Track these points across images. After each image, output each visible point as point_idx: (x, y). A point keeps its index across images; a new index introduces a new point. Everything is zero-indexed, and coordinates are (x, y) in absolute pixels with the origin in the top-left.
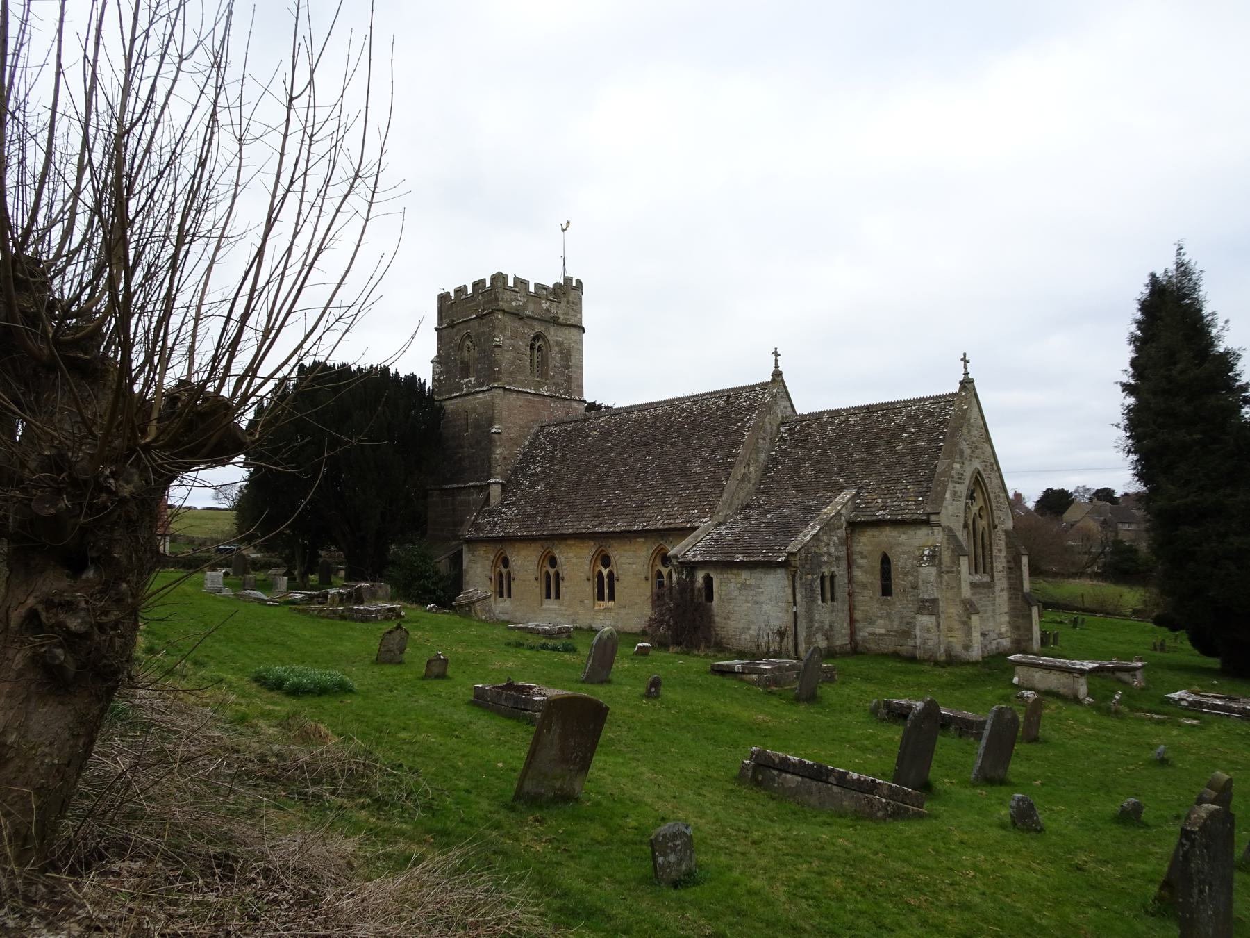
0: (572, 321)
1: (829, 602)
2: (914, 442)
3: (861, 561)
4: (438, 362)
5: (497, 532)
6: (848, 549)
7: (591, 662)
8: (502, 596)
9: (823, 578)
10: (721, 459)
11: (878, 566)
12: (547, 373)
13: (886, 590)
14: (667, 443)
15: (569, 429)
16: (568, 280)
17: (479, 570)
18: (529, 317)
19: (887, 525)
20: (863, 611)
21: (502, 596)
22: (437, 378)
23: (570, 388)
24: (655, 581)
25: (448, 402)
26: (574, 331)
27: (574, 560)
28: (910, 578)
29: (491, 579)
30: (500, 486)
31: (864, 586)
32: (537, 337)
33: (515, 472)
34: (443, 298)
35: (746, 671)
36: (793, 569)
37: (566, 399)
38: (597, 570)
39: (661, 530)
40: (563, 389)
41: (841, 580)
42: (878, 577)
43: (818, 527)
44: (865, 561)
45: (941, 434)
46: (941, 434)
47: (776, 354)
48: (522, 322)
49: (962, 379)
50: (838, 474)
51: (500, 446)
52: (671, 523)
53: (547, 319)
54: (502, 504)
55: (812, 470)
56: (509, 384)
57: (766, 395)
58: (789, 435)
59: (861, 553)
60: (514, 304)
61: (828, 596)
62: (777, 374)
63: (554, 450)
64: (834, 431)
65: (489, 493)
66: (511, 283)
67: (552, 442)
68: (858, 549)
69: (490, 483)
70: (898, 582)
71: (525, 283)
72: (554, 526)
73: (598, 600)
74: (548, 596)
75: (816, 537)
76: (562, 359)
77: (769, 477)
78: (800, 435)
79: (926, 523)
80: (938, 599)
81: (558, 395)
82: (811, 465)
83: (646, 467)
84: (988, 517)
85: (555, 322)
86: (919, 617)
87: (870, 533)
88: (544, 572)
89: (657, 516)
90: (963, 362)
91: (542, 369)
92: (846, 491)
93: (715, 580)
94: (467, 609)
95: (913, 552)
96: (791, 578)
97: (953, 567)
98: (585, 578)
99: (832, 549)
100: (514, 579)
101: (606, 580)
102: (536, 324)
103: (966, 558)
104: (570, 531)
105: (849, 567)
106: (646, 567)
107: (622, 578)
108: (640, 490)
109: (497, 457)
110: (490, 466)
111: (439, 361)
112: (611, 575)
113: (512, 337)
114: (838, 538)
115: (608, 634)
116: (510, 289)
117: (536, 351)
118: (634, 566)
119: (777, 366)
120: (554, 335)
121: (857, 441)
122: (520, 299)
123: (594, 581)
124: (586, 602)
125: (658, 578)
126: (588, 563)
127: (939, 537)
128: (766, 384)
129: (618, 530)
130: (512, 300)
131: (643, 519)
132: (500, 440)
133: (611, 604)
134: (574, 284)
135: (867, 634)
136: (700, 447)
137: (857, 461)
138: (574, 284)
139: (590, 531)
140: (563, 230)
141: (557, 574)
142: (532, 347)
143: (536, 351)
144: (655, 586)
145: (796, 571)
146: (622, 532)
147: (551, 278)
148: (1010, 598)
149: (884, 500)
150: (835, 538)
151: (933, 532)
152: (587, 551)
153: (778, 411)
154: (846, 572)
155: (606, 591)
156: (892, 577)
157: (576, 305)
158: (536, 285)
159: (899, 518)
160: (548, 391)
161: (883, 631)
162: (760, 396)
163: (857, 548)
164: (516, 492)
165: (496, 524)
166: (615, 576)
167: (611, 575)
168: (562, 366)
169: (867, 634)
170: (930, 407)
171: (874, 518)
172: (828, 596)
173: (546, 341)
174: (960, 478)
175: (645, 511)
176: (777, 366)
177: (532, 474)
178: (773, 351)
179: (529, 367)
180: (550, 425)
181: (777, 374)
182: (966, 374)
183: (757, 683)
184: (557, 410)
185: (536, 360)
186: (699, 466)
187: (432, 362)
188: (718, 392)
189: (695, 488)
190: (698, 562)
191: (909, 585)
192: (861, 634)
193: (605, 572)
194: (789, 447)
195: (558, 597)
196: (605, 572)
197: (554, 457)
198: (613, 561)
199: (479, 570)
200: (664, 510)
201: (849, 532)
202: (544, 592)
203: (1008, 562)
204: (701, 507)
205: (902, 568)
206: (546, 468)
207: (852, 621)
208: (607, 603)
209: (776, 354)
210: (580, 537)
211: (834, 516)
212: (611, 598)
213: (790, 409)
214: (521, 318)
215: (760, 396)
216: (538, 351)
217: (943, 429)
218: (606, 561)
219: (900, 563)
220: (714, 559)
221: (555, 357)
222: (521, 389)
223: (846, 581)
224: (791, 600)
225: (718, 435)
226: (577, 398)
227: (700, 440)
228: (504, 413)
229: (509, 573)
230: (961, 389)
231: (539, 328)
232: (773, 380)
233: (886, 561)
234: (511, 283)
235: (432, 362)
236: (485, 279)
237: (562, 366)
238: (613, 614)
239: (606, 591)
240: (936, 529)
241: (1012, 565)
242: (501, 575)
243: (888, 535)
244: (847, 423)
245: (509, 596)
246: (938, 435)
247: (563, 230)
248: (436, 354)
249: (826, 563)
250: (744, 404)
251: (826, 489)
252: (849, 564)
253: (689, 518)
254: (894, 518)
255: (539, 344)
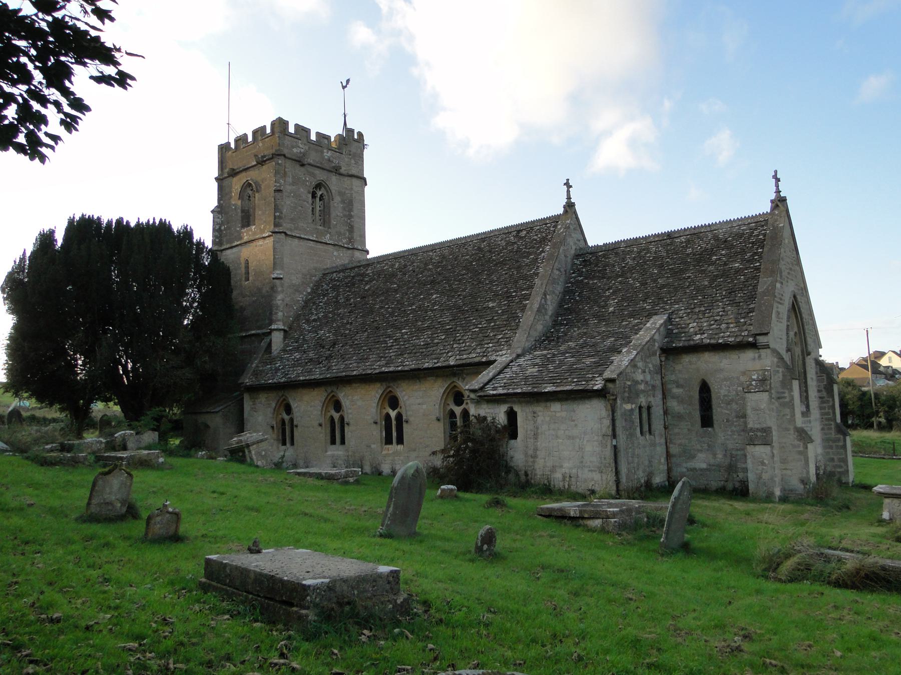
0: (354, 171)
1: (648, 436)
2: (725, 264)
3: (676, 391)
4: (219, 212)
5: (280, 378)
6: (662, 378)
7: (391, 509)
8: (284, 444)
9: (640, 408)
10: (515, 292)
11: (696, 395)
12: (330, 222)
13: (707, 420)
14: (455, 280)
15: (352, 275)
16: (350, 131)
17: (260, 419)
18: (309, 164)
19: (706, 351)
20: (680, 445)
21: (284, 444)
22: (217, 227)
23: (352, 238)
24: (448, 420)
25: (229, 252)
26: (355, 182)
27: (360, 403)
28: (734, 406)
29: (273, 427)
30: (282, 333)
31: (680, 417)
32: (319, 186)
33: (297, 318)
34: (224, 149)
35: (586, 516)
36: (612, 398)
37: (348, 248)
38: (385, 412)
39: (453, 366)
40: (346, 238)
41: (657, 411)
42: (697, 407)
43: (635, 352)
44: (681, 390)
45: (756, 254)
46: (756, 254)
47: (568, 185)
48: (302, 169)
49: (773, 198)
50: (644, 301)
51: (283, 291)
52: (466, 358)
53: (328, 168)
54: (284, 350)
55: (614, 299)
56: (291, 230)
57: (559, 227)
58: (585, 266)
59: (674, 382)
60: (295, 150)
61: (646, 428)
62: (570, 206)
63: (338, 295)
64: (634, 259)
65: (271, 340)
66: (292, 130)
67: (335, 288)
68: (673, 377)
69: (272, 330)
70: (719, 411)
71: (307, 131)
72: (337, 368)
73: (386, 444)
74: (333, 442)
75: (632, 364)
76: (344, 209)
77: (565, 309)
78: (596, 265)
79: (753, 346)
80: (770, 428)
81: (340, 244)
82: (612, 294)
83: (434, 304)
84: (802, 345)
85: (336, 171)
86: (750, 449)
87: (686, 359)
88: (328, 417)
89: (448, 352)
90: (778, 177)
91: (325, 218)
92: (655, 317)
93: (518, 415)
94: (241, 454)
95: (738, 378)
96: (609, 407)
97: (784, 393)
98: (372, 421)
99: (648, 377)
100: (297, 426)
101: (394, 422)
102: (317, 172)
103: (797, 381)
104: (355, 373)
105: (664, 397)
106: (437, 407)
107: (411, 419)
108: (428, 328)
109: (279, 303)
110: (271, 314)
111: (219, 211)
112: (399, 417)
113: (293, 184)
114: (653, 366)
115: (412, 471)
116: (290, 135)
117: (318, 199)
118: (424, 407)
119: (569, 198)
120: (334, 182)
121: (661, 266)
122: (301, 146)
123: (381, 424)
124: (373, 446)
125: (451, 418)
126: (375, 405)
127: (767, 361)
128: (559, 216)
129: (406, 369)
130: (293, 147)
131: (433, 356)
132: (282, 285)
133: (400, 447)
134: (356, 137)
135: (685, 470)
136: (491, 282)
137: (663, 286)
138: (356, 137)
139: (377, 371)
140: (344, 87)
141: (342, 419)
142: (314, 196)
143: (318, 199)
144: (448, 426)
145: (615, 400)
146: (412, 370)
147: (334, 130)
148: (823, 429)
149: (700, 324)
150: (650, 366)
151: (760, 356)
152: (373, 393)
153: (572, 243)
154: (661, 403)
155: (394, 434)
156: (714, 407)
157: (359, 158)
158: (318, 134)
159: (720, 341)
160: (330, 239)
161: (704, 466)
162: (552, 229)
163: (671, 377)
164: (299, 338)
165: (277, 370)
166: (404, 418)
167: (399, 417)
168: (345, 216)
169: (685, 470)
170: (739, 229)
171: (692, 343)
172: (646, 428)
173: (328, 190)
174: (781, 299)
175: (434, 348)
176: (569, 198)
177: (315, 320)
178: (565, 182)
179: (311, 215)
180: (333, 273)
181: (570, 206)
182: (778, 192)
183: (603, 530)
184: (340, 258)
185: (318, 208)
186: (491, 300)
187: (213, 212)
188: (506, 228)
189: (489, 322)
190: (500, 395)
191: (734, 414)
192: (679, 470)
193: (393, 414)
194: (586, 278)
195: (343, 442)
196: (393, 414)
197: (337, 302)
198: (401, 403)
199: (260, 418)
200: (455, 346)
201: (663, 359)
202: (329, 438)
203: (819, 391)
204: (496, 341)
205: (725, 396)
206: (330, 312)
207: (668, 455)
208: (394, 447)
209: (568, 185)
210: (366, 379)
211: (648, 341)
212: (400, 441)
213: (582, 242)
214: (303, 165)
215: (552, 229)
216: (320, 200)
217: (757, 249)
218: (394, 403)
219: (720, 391)
220: (519, 391)
221: (337, 209)
222: (302, 236)
223: (662, 412)
224: (610, 432)
225: (509, 269)
226: (360, 248)
227: (489, 275)
228: (285, 259)
229: (292, 420)
230: (773, 209)
231: (321, 176)
232: (566, 212)
233: (705, 389)
234: (292, 130)
235: (213, 212)
236: (265, 126)
237: (345, 216)
238: (402, 458)
239: (394, 434)
240: (763, 352)
241: (824, 394)
242: (283, 421)
243: (707, 363)
244: (648, 250)
245: (292, 444)
246: (753, 256)
247: (344, 87)
248: (216, 204)
249: (643, 391)
250: (535, 237)
251: (632, 315)
252: (664, 394)
253: (484, 352)
254: (713, 341)
255: (320, 193)
